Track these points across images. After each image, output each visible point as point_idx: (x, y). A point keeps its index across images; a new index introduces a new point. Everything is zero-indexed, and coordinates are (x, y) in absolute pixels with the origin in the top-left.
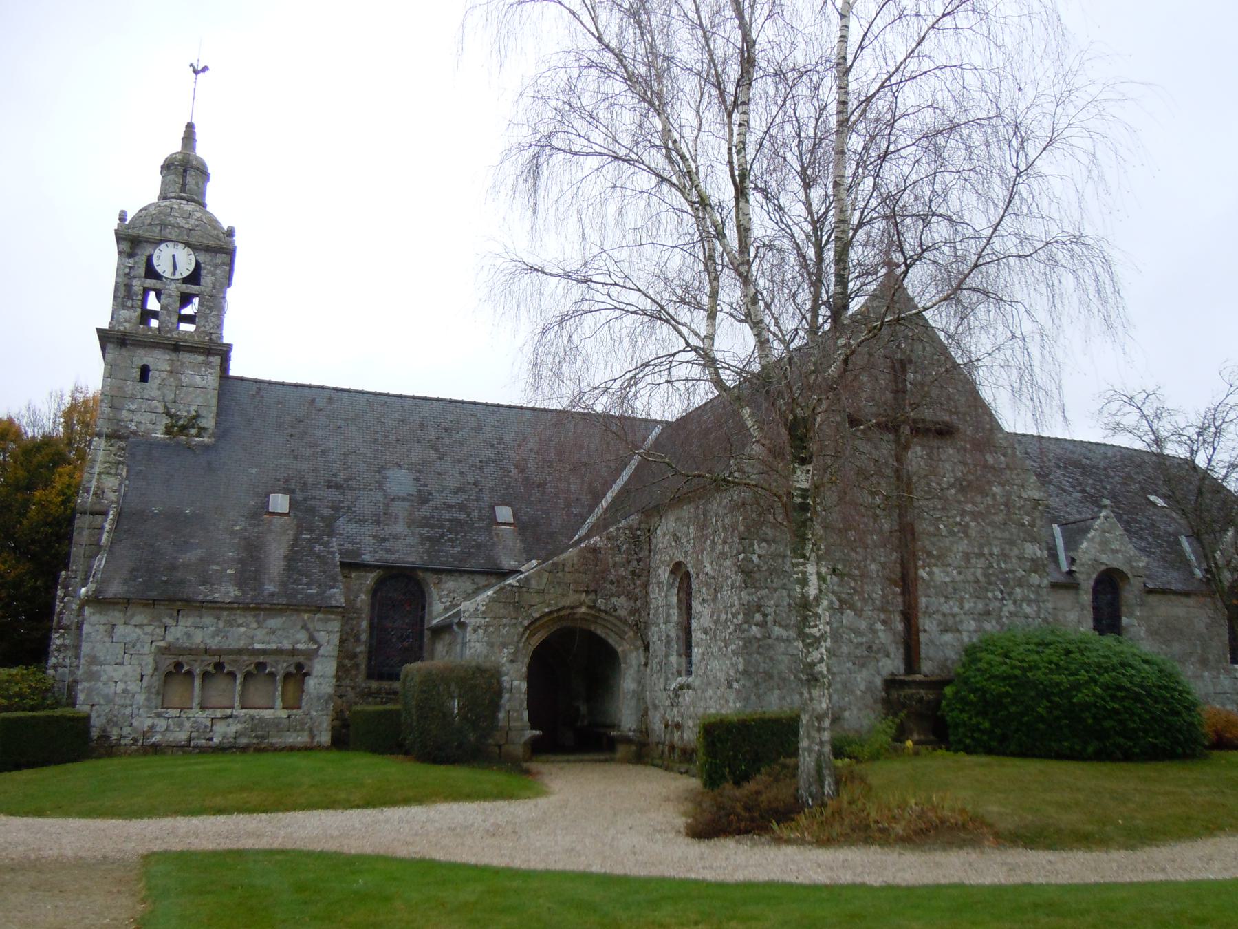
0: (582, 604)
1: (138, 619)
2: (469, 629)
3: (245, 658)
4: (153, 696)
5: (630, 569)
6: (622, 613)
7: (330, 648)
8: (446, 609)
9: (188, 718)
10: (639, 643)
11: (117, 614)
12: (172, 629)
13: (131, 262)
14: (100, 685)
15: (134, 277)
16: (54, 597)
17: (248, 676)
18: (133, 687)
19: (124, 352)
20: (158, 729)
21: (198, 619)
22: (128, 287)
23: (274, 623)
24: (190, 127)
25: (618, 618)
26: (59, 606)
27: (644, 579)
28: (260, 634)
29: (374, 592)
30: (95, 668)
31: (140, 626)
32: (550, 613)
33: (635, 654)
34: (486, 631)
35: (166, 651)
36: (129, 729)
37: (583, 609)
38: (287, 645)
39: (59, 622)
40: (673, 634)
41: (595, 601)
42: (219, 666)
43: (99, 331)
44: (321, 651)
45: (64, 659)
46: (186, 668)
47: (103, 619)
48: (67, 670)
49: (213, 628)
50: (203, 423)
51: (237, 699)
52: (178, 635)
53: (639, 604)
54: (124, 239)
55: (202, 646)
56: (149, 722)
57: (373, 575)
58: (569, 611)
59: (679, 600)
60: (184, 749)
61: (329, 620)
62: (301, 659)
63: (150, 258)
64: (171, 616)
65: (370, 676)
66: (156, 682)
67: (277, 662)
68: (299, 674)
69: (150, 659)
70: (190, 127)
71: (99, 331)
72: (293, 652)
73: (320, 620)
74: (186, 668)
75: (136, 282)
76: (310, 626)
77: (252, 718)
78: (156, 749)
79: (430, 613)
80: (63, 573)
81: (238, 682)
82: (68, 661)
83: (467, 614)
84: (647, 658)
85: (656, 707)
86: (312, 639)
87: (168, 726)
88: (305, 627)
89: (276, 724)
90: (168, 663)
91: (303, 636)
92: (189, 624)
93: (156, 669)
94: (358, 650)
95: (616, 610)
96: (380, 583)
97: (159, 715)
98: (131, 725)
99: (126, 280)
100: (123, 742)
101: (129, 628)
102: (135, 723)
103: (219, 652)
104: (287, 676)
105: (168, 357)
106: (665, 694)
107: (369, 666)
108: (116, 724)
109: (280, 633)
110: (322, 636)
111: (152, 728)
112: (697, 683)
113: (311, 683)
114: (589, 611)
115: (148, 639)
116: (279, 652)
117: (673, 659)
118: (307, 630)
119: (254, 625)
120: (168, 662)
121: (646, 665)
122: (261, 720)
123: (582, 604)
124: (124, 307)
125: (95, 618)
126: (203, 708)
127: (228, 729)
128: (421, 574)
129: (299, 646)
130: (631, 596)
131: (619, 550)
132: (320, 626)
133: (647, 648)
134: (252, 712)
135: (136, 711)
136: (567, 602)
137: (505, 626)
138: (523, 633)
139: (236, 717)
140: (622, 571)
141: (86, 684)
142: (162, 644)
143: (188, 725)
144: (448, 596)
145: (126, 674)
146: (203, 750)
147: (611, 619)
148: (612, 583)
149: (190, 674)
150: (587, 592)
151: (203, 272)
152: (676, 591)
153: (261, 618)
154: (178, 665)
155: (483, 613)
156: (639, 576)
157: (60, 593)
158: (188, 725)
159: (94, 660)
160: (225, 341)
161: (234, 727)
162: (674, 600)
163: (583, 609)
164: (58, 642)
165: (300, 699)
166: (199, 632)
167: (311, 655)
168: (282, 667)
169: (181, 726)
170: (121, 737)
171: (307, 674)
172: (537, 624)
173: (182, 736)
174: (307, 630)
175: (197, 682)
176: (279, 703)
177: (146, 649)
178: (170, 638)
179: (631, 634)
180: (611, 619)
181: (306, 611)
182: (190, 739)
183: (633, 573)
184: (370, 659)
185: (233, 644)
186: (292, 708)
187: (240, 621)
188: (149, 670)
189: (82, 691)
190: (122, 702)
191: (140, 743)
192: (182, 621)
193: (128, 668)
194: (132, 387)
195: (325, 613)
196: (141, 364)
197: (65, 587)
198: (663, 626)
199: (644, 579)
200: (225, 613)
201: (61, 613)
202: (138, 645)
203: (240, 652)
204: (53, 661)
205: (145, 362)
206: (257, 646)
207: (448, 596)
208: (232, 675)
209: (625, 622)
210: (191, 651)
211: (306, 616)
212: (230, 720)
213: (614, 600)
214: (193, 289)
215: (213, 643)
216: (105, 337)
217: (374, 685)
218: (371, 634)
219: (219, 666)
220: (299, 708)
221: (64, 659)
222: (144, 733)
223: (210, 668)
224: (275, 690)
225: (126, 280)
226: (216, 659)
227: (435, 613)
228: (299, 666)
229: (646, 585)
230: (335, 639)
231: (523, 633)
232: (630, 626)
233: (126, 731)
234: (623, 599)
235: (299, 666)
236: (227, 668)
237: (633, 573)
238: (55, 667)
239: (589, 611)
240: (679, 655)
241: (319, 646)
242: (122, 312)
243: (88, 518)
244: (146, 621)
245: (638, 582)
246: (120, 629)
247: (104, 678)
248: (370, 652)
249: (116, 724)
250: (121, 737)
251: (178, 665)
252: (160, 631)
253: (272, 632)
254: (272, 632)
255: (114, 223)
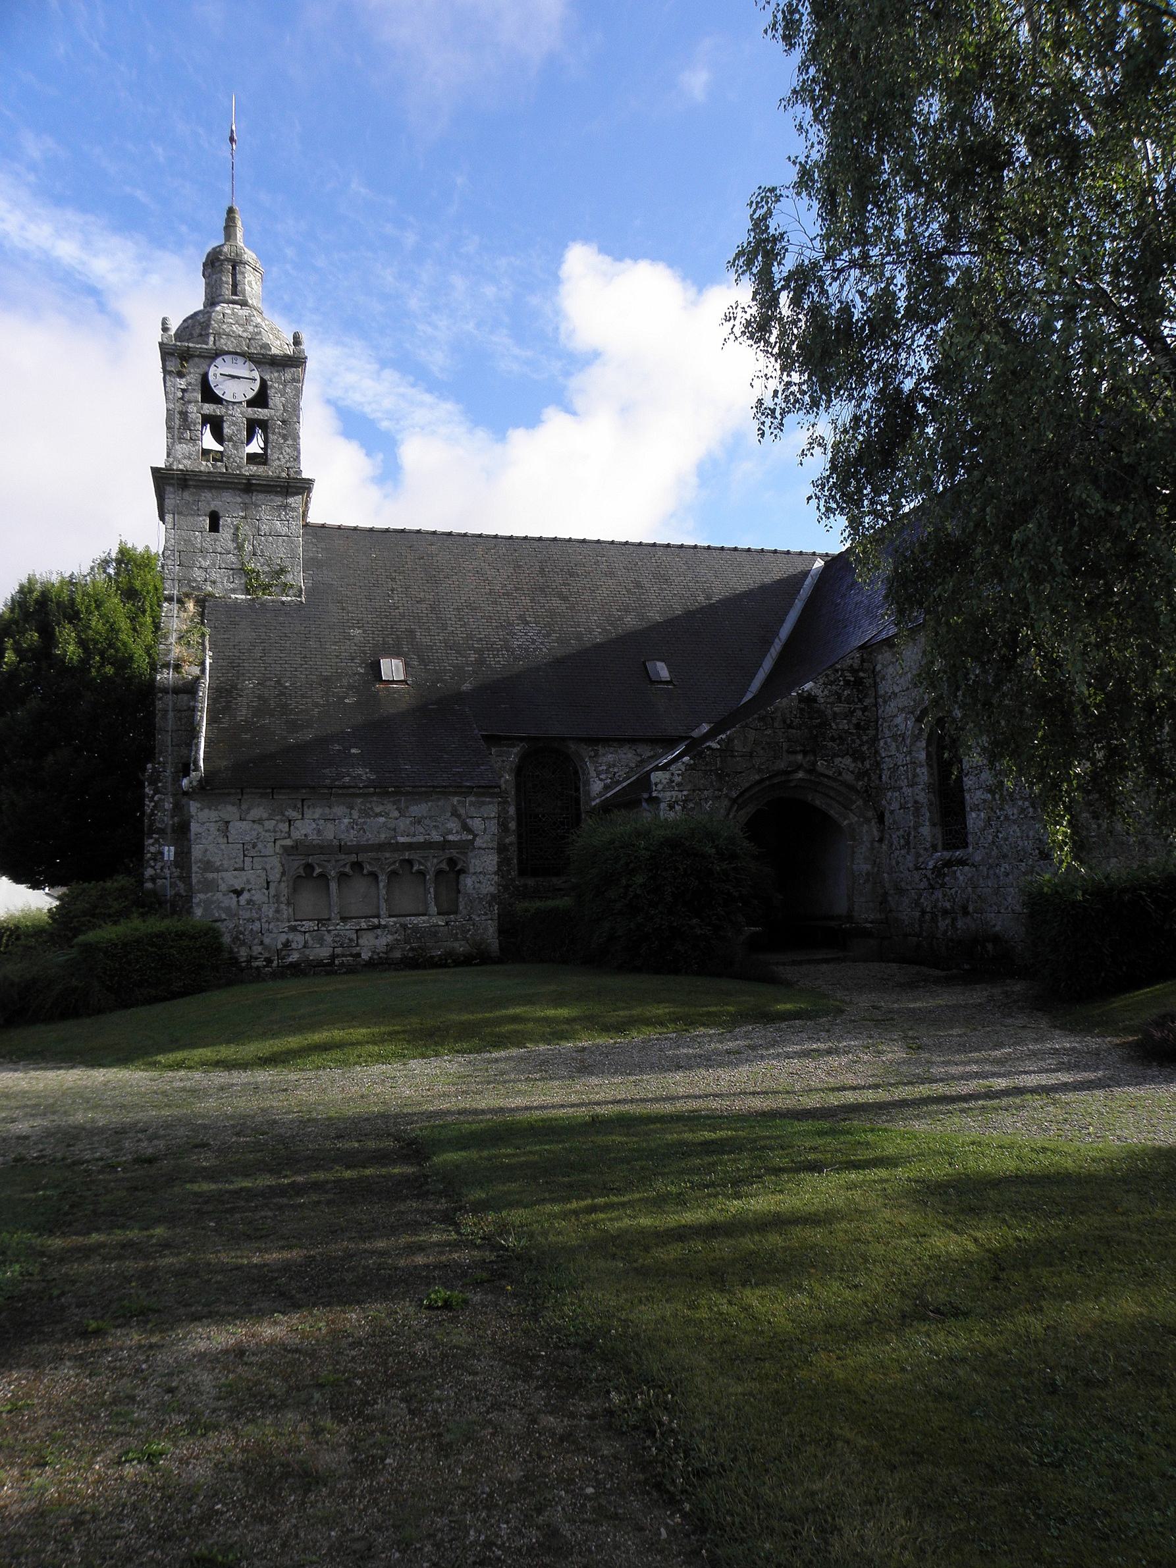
0: (800, 767)
1: (257, 813)
2: (663, 806)
3: (388, 855)
4: (283, 907)
5: (854, 721)
6: (849, 778)
7: (487, 837)
8: (607, 788)
9: (329, 931)
10: (870, 814)
11: (230, 808)
12: (298, 824)
13: (182, 383)
14: (219, 895)
15: (190, 402)
16: (143, 796)
17: (342, 877)
18: (259, 897)
19: (186, 495)
20: (294, 946)
21: (327, 810)
22: (184, 415)
23: (419, 809)
24: (231, 211)
25: (844, 783)
26: (149, 806)
27: (872, 732)
28: (403, 824)
29: (519, 772)
30: (210, 876)
31: (259, 821)
32: (762, 781)
33: (865, 828)
34: (684, 807)
35: (289, 851)
36: (260, 948)
37: (801, 775)
38: (436, 837)
39: (151, 825)
40: (922, 797)
41: (814, 763)
42: (358, 866)
43: (155, 471)
44: (479, 842)
45: (162, 869)
46: (318, 870)
47: (213, 815)
48: (167, 883)
49: (346, 821)
50: (289, 578)
51: (383, 905)
52: (309, 831)
53: (867, 764)
54: (172, 354)
55: (336, 842)
56: (283, 938)
57: (515, 750)
58: (783, 778)
59: (928, 755)
60: (327, 968)
61: (484, 803)
62: (454, 853)
63: (205, 379)
64: (295, 808)
65: (522, 873)
66: (284, 889)
67: (426, 858)
68: (453, 871)
69: (275, 862)
70: (231, 211)
71: (155, 471)
72: (445, 845)
73: (472, 803)
74: (318, 870)
75: (192, 408)
76: (462, 811)
77: (404, 927)
78: (296, 970)
79: (588, 793)
80: (149, 766)
81: (381, 885)
82: (166, 871)
83: (660, 787)
84: (882, 831)
85: (901, 891)
86: (466, 828)
87: (306, 942)
88: (455, 814)
89: (433, 932)
90: (297, 864)
91: (453, 825)
92: (316, 816)
93: (283, 874)
94: (507, 841)
95: (840, 774)
96: (524, 758)
97: (293, 929)
98: (262, 943)
99: (178, 406)
100: (255, 964)
101: (244, 825)
102: (267, 941)
103: (359, 849)
104: (439, 873)
105: (239, 500)
106: (917, 876)
107: (520, 862)
108: (243, 943)
109: (427, 821)
110: (477, 824)
111: (287, 944)
112: (978, 858)
113: (468, 882)
114: (808, 777)
115: (270, 837)
116: (428, 845)
117: (926, 830)
118: (459, 816)
119: (396, 814)
120: (296, 864)
121: (881, 840)
122: (416, 929)
123: (800, 767)
124: (181, 439)
125: (205, 814)
126: (344, 919)
127: (377, 942)
128: (573, 746)
129: (450, 838)
130: (858, 756)
131: (839, 698)
132: (473, 811)
133: (881, 819)
134: (402, 920)
135: (265, 926)
136: (781, 765)
137: (706, 800)
138: (731, 807)
139: (385, 926)
140: (844, 725)
141: (201, 896)
142: (288, 842)
143: (329, 939)
144: (607, 771)
145: (248, 882)
146: (351, 970)
147: (834, 785)
148: (833, 739)
149: (323, 876)
150: (805, 753)
151: (271, 392)
152: (924, 744)
153: (403, 805)
154: (309, 867)
155: (679, 784)
156: (864, 730)
157: (148, 790)
158: (329, 939)
159: (208, 866)
160: (304, 476)
161: (383, 941)
162: (923, 756)
163: (801, 775)
164: (152, 849)
165: (456, 902)
166: (330, 825)
167: (466, 847)
168: (432, 864)
169: (321, 941)
170: (251, 958)
171: (462, 871)
172: (747, 795)
173: (324, 953)
174: (459, 816)
175: (333, 886)
176: (433, 909)
177: (269, 851)
178: (297, 835)
179: (860, 802)
180: (834, 785)
181: (455, 794)
182: (333, 957)
183: (857, 726)
184: (520, 851)
185: (371, 837)
186: (448, 914)
187: (378, 810)
188: (275, 875)
189: (198, 904)
190: (247, 915)
191: (275, 964)
192: (309, 813)
193: (249, 874)
194: (201, 537)
195: (477, 795)
196: (208, 510)
197: (153, 782)
198: (908, 791)
199: (872, 732)
200: (359, 800)
201: (153, 814)
202: (260, 846)
203: (381, 847)
204: (149, 872)
205: (212, 508)
206: (401, 839)
207: (607, 771)
208: (374, 876)
209: (851, 788)
210: (322, 849)
211: (455, 800)
212: (379, 931)
213: (837, 760)
214: (261, 413)
215: (351, 838)
216: (162, 478)
217: (531, 882)
218: (519, 825)
219: (358, 866)
220: (456, 912)
221: (162, 869)
222: (278, 951)
223: (347, 869)
224: (427, 891)
225: (178, 406)
226: (353, 858)
227: (593, 794)
228: (452, 862)
229: (875, 740)
230: (494, 827)
231: (731, 807)
232: (857, 792)
233: (257, 949)
234: (848, 761)
235: (452, 862)
236: (367, 868)
237: (857, 726)
238: (153, 879)
239: (808, 777)
240: (934, 825)
241: (475, 836)
242: (178, 447)
243: (170, 697)
244: (265, 815)
245: (865, 738)
246: (237, 827)
247: (223, 887)
248: (519, 843)
249: (243, 943)
250: (251, 958)
251: (309, 867)
252: (284, 827)
253: (418, 821)
254: (418, 821)
255: (157, 336)
